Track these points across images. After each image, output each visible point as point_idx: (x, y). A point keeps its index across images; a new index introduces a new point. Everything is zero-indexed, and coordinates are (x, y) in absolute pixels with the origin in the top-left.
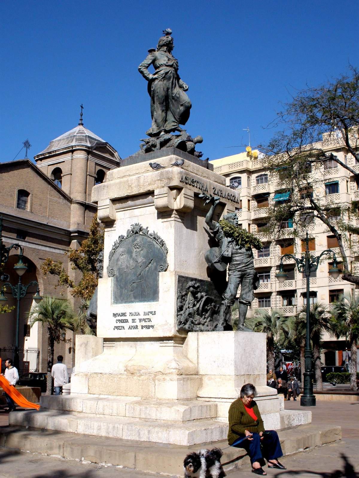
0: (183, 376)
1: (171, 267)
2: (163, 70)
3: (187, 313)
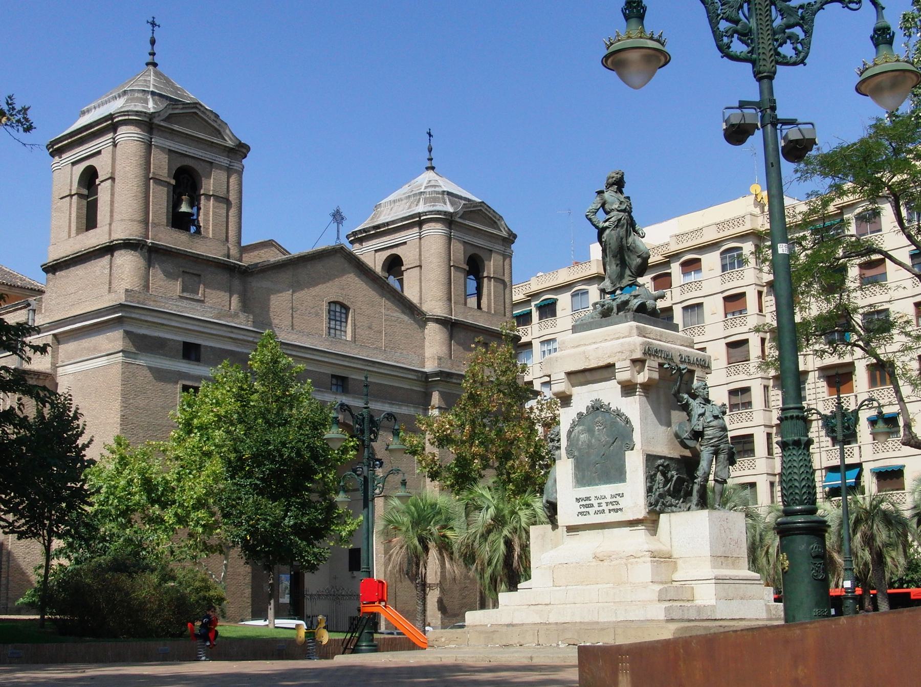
0: (657, 559)
1: (638, 446)
2: (615, 216)
3: (657, 493)
